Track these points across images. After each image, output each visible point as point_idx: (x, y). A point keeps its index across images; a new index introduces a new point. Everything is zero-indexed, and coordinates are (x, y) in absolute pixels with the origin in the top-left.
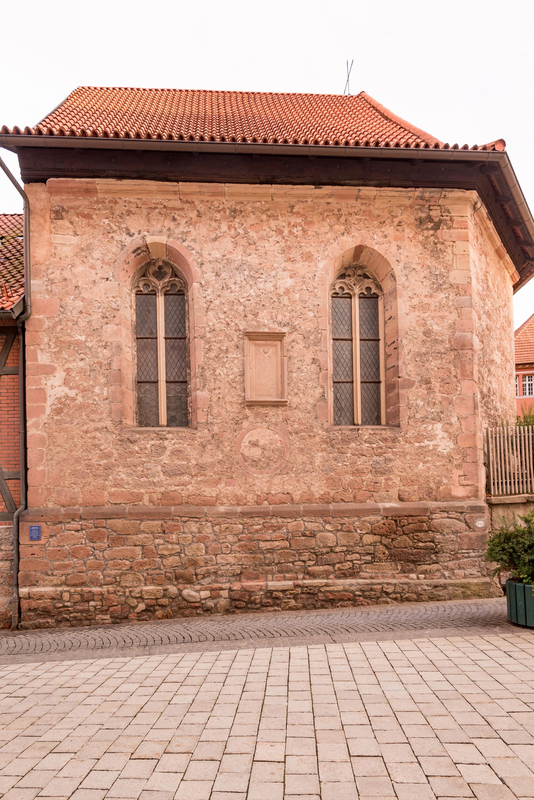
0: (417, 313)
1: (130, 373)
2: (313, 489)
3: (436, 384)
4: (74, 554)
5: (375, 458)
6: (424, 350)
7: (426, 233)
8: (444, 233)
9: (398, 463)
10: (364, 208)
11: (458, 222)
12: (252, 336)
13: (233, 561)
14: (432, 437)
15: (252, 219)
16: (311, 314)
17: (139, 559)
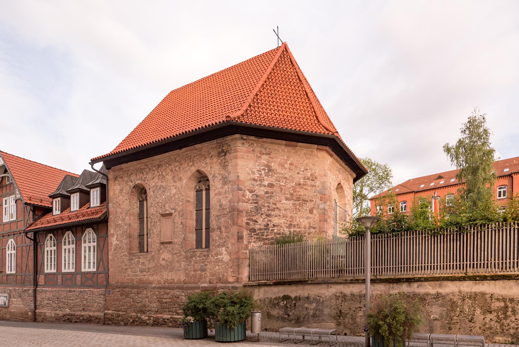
0: (217, 197)
1: (136, 234)
2: (181, 278)
3: (223, 229)
4: (117, 300)
5: (202, 264)
6: (219, 214)
7: (221, 158)
8: (228, 156)
9: (209, 266)
10: (199, 153)
11: (234, 150)
12: (163, 215)
13: (155, 306)
14: (221, 254)
15: (164, 167)
16: (181, 203)
17: (132, 303)
